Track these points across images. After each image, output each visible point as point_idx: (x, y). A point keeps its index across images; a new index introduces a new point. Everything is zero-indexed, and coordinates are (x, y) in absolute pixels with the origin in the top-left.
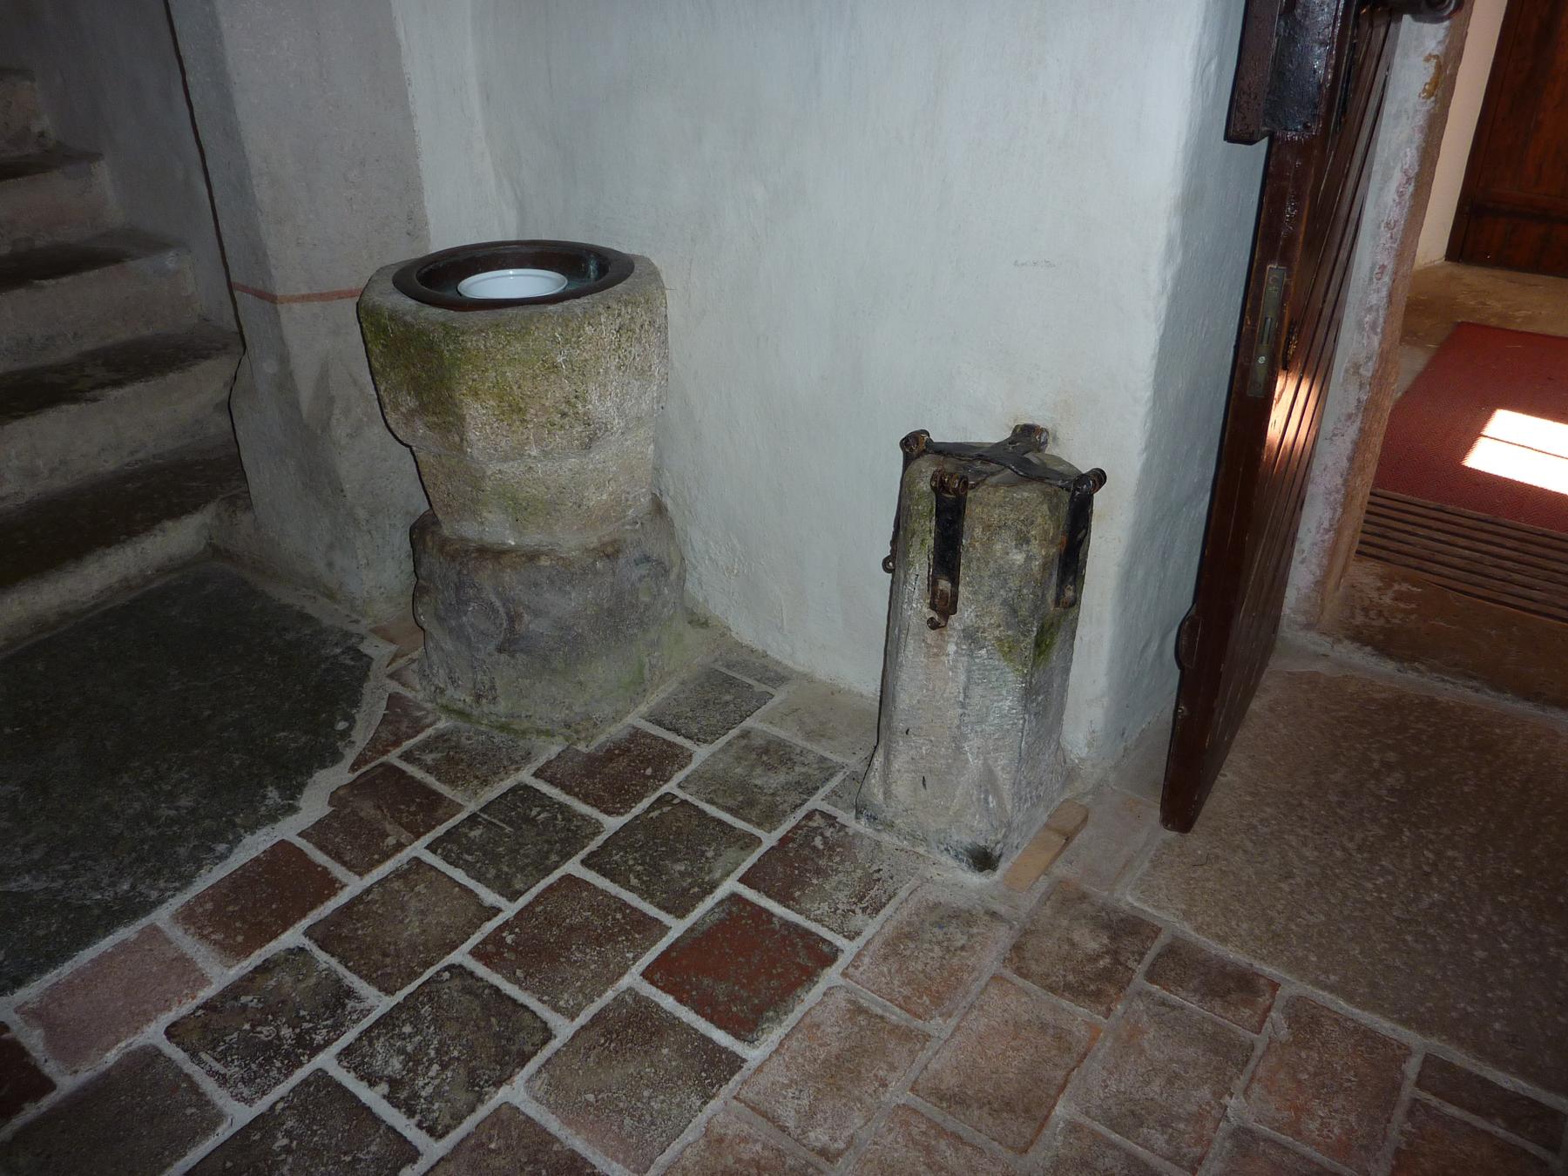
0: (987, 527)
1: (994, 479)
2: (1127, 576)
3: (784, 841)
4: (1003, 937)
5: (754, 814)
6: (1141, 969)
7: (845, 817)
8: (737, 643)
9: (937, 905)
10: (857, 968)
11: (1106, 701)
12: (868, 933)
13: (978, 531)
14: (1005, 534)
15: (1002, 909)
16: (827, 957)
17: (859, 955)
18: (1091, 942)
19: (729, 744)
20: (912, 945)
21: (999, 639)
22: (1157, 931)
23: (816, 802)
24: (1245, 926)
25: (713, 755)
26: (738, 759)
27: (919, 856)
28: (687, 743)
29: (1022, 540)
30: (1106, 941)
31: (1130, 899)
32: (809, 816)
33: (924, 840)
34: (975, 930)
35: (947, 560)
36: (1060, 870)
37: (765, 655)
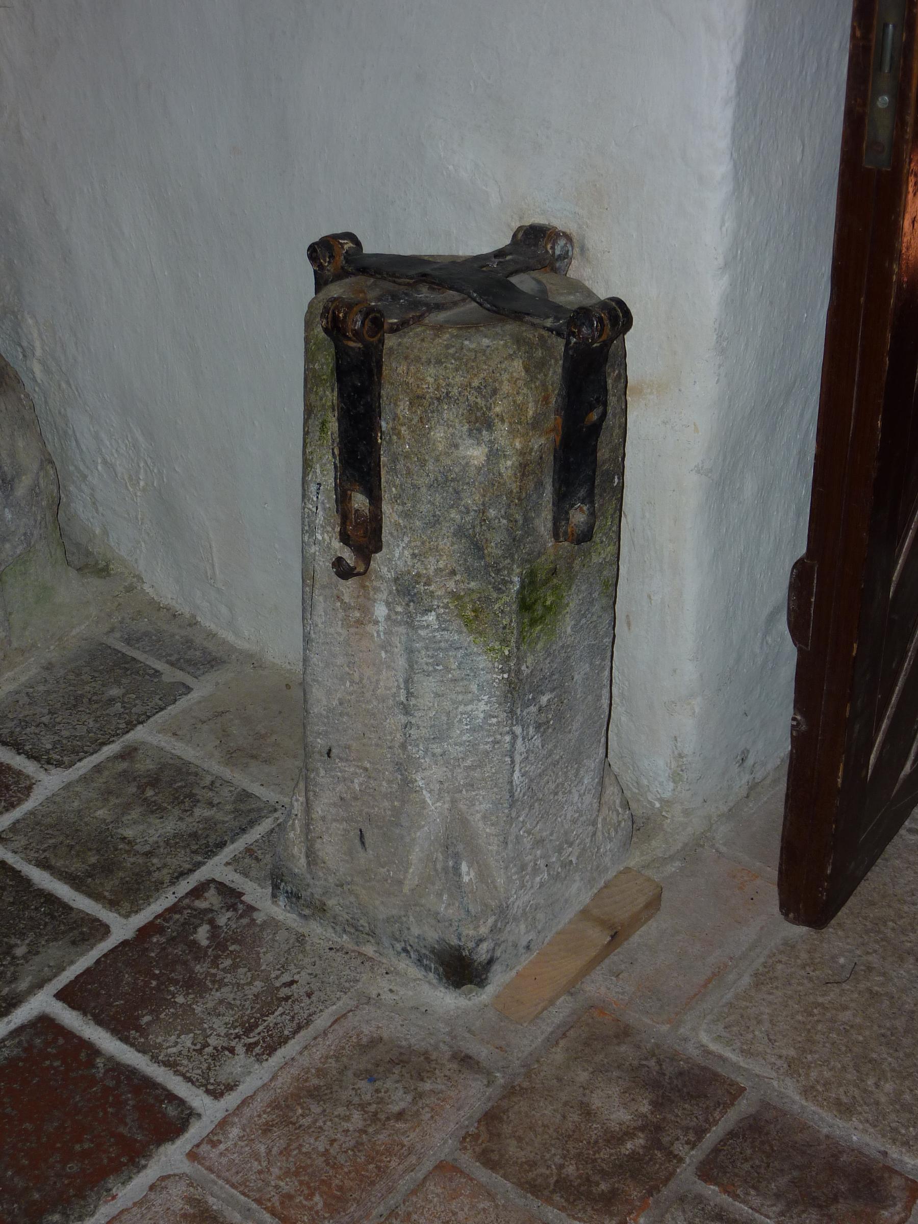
0: (417, 399)
1: (441, 316)
2: (722, 482)
3: (144, 932)
4: (474, 1096)
5: (108, 886)
6: (693, 1157)
7: (256, 893)
8: (152, 602)
9: (375, 1042)
10: (214, 1144)
11: (697, 704)
12: (245, 1089)
13: (403, 408)
14: (449, 413)
15: (482, 1052)
16: (163, 1120)
17: (223, 1124)
18: (617, 1108)
19: (98, 769)
20: (316, 1109)
21: (455, 596)
22: (736, 1093)
23: (216, 868)
24: (888, 1087)
25: (67, 787)
26: (107, 794)
27: (365, 959)
28: (29, 767)
29: (480, 422)
30: (645, 1108)
31: (704, 1038)
32: (198, 892)
33: (372, 933)
34: (427, 1086)
35: (358, 454)
36: (598, 986)
37: (193, 623)
